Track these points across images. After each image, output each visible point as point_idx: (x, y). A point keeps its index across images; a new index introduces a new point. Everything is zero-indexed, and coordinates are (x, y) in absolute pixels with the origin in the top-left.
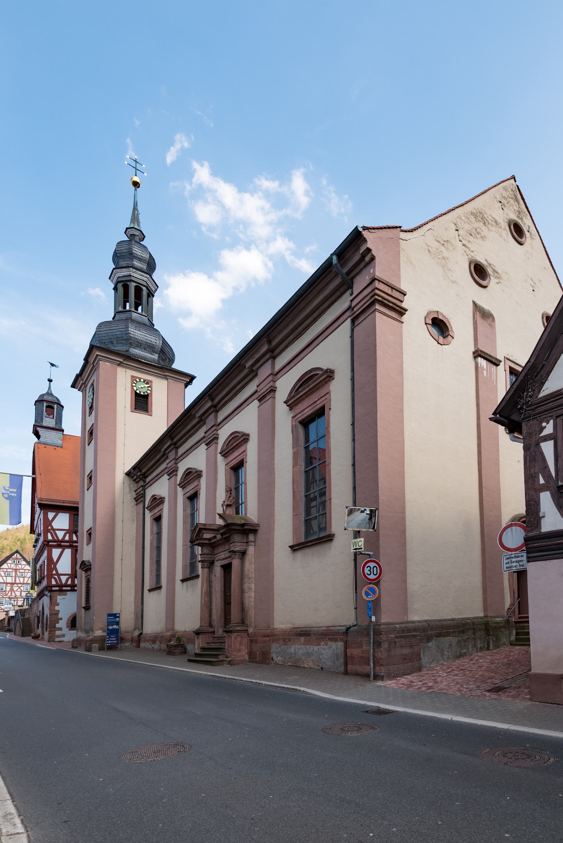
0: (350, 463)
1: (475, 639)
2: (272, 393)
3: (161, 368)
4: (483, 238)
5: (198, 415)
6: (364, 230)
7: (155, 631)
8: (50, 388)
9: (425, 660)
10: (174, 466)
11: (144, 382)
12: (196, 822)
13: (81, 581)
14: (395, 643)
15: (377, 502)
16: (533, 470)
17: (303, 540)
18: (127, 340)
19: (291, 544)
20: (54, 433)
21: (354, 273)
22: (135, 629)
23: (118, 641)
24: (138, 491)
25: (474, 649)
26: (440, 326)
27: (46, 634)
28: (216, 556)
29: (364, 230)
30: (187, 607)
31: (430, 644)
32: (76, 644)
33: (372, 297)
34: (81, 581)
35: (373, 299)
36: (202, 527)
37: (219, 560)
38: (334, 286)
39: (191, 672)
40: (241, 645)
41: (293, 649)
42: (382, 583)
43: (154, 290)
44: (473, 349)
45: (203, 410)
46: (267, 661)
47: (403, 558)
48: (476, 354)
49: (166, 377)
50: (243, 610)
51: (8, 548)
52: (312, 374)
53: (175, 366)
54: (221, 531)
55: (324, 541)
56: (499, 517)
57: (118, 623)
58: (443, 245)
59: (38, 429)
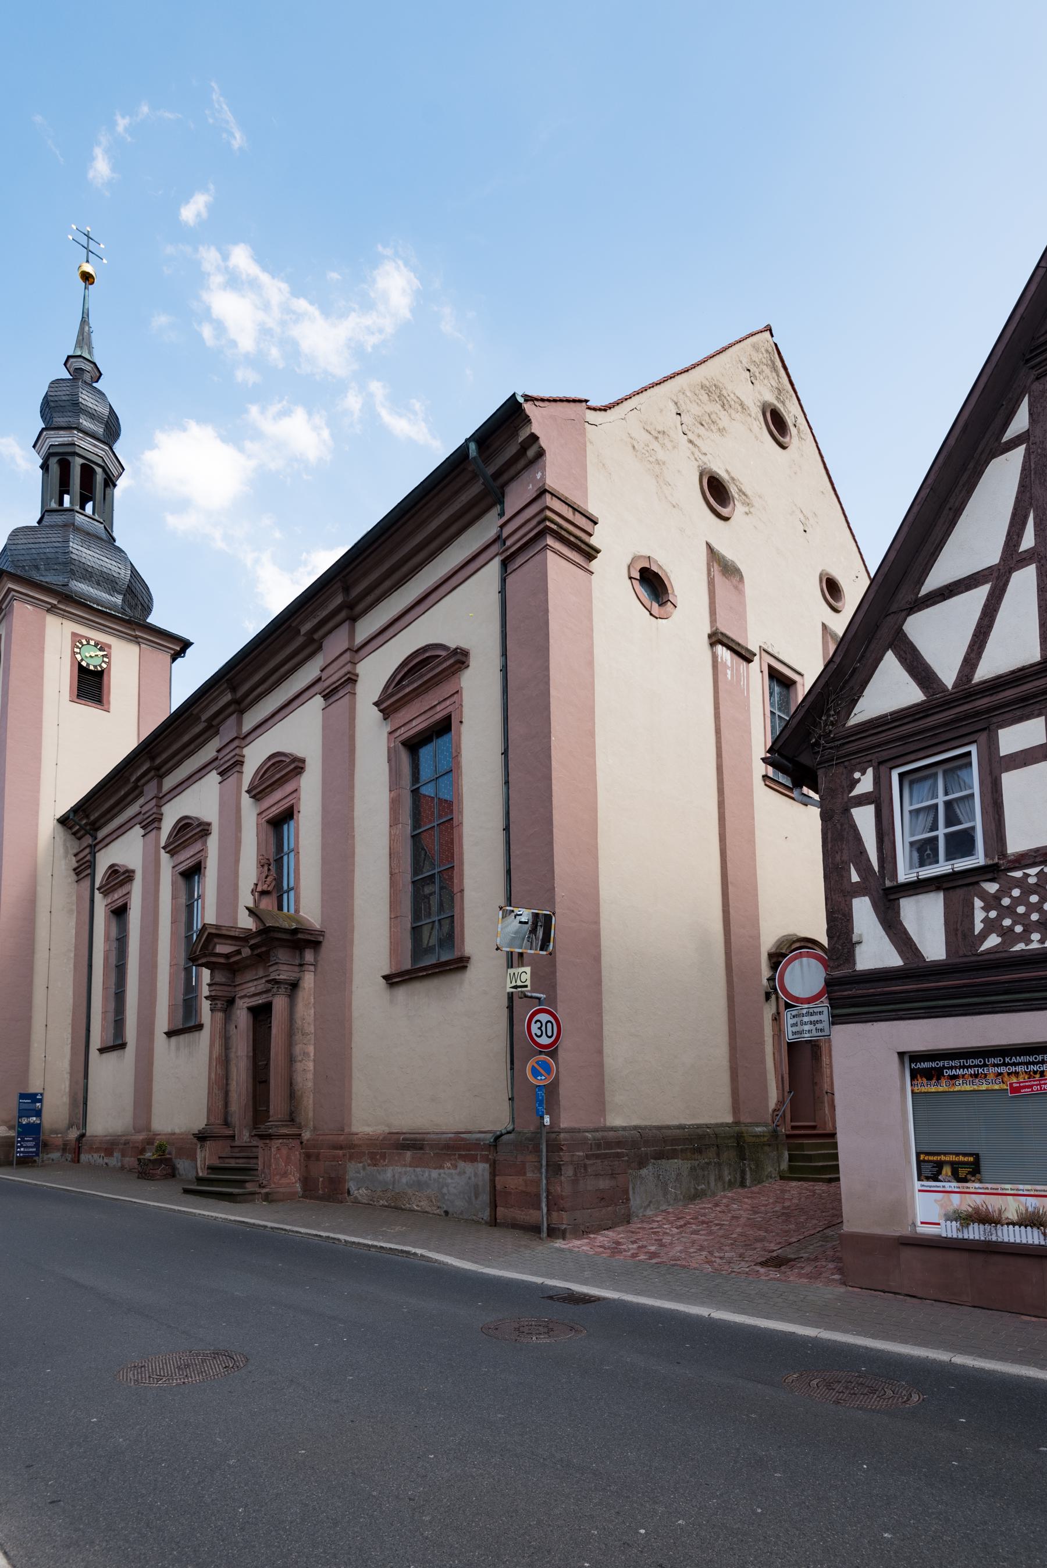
0: (500, 824)
1: (719, 1164)
2: (350, 686)
3: (129, 623)
4: (722, 431)
5: (204, 717)
6: (526, 401)
7: (111, 1131)
9: (636, 1201)
11: (96, 645)
12: (307, 1505)
14: (585, 1166)
15: (551, 900)
16: (838, 858)
17: (407, 965)
19: (386, 972)
21: (505, 477)
22: (71, 1126)
23: (38, 1149)
24: (81, 855)
25: (719, 1184)
26: (652, 583)
28: (238, 989)
29: (526, 401)
30: (182, 1087)
31: (644, 1172)
33: (539, 523)
35: (541, 526)
36: (214, 931)
37: (245, 996)
38: (470, 497)
39: (195, 1214)
40: (287, 1164)
41: (389, 1175)
42: (561, 1053)
43: (116, 473)
44: (708, 630)
45: (214, 709)
46: (340, 1196)
47: (596, 1008)
48: (714, 639)
49: (136, 640)
50: (292, 1095)
52: (427, 655)
53: (154, 619)
54: (252, 942)
55: (450, 970)
56: (757, 937)
57: (38, 1113)
58: (657, 438)
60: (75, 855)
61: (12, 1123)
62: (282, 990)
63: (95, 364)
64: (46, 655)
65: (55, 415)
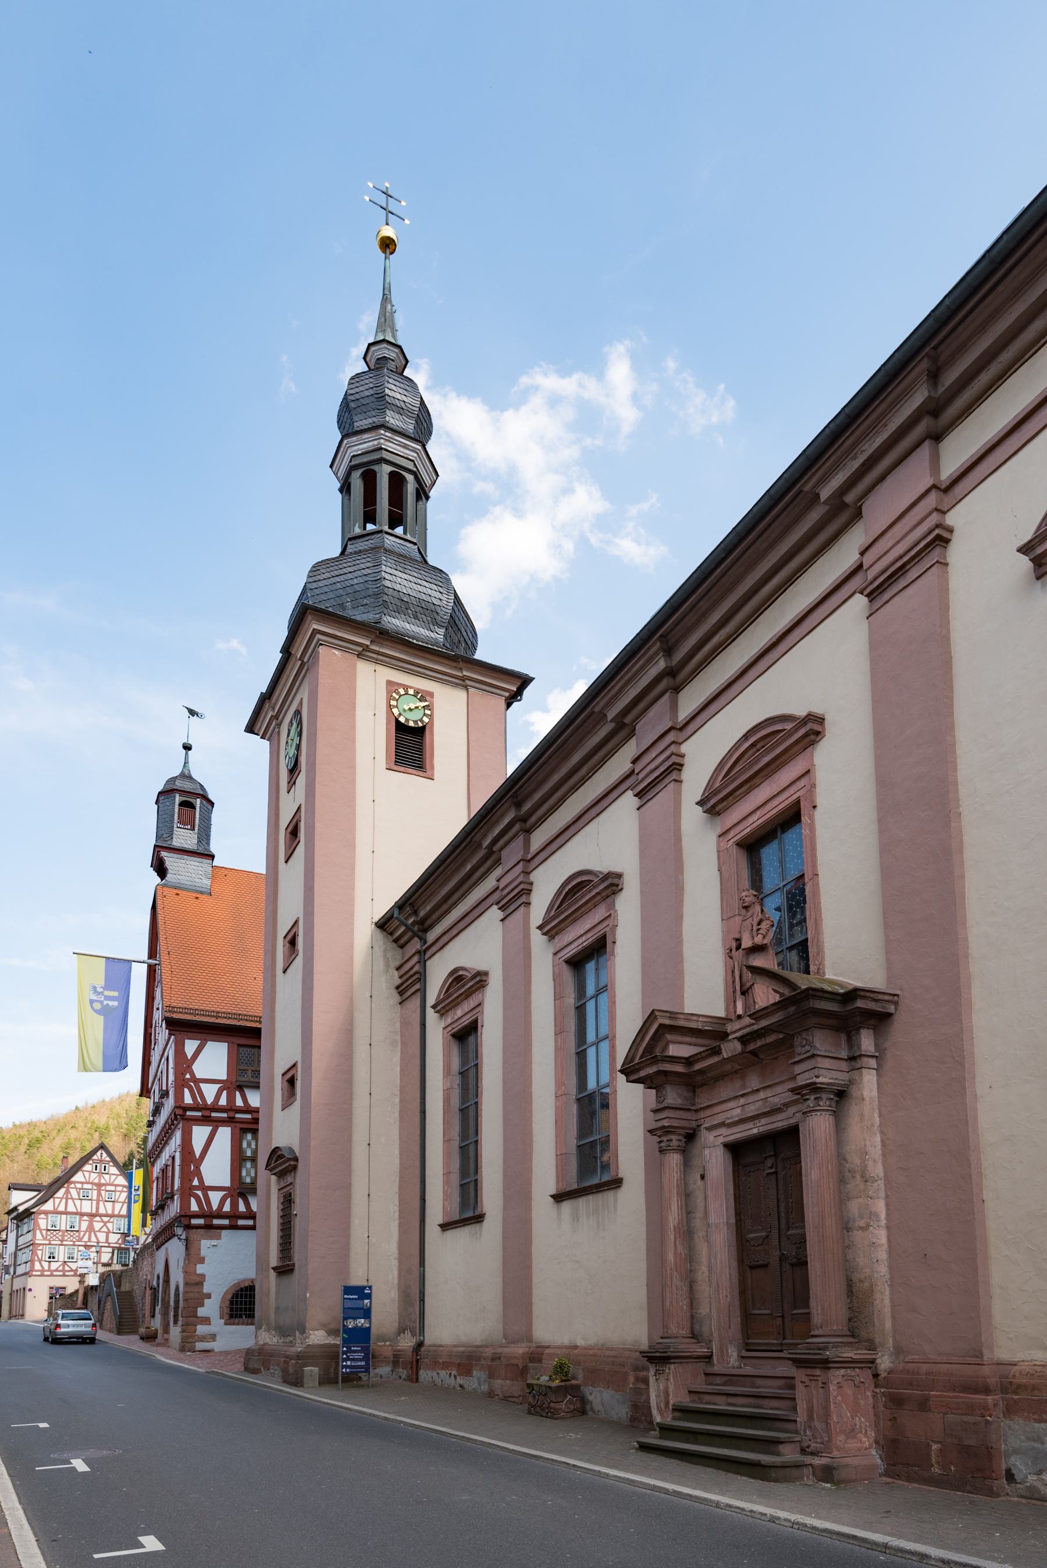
2: (938, 551)
5: (611, 714)
7: (464, 1339)
8: (186, 763)
10: (521, 879)
11: (417, 693)
13: (267, 1202)
18: (374, 601)
20: (194, 863)
22: (402, 1330)
23: (368, 1364)
27: (175, 1332)
28: (702, 1114)
32: (255, 1360)
34: (267, 1202)
36: (667, 1022)
43: (428, 482)
49: (462, 683)
51: (78, 1145)
53: (481, 654)
57: (367, 1313)
59: (163, 854)
60: (398, 969)
61: (333, 1326)
62: (824, 1104)
63: (400, 347)
64: (357, 712)
65: (355, 418)
